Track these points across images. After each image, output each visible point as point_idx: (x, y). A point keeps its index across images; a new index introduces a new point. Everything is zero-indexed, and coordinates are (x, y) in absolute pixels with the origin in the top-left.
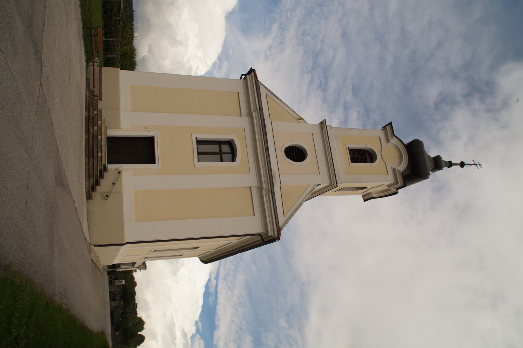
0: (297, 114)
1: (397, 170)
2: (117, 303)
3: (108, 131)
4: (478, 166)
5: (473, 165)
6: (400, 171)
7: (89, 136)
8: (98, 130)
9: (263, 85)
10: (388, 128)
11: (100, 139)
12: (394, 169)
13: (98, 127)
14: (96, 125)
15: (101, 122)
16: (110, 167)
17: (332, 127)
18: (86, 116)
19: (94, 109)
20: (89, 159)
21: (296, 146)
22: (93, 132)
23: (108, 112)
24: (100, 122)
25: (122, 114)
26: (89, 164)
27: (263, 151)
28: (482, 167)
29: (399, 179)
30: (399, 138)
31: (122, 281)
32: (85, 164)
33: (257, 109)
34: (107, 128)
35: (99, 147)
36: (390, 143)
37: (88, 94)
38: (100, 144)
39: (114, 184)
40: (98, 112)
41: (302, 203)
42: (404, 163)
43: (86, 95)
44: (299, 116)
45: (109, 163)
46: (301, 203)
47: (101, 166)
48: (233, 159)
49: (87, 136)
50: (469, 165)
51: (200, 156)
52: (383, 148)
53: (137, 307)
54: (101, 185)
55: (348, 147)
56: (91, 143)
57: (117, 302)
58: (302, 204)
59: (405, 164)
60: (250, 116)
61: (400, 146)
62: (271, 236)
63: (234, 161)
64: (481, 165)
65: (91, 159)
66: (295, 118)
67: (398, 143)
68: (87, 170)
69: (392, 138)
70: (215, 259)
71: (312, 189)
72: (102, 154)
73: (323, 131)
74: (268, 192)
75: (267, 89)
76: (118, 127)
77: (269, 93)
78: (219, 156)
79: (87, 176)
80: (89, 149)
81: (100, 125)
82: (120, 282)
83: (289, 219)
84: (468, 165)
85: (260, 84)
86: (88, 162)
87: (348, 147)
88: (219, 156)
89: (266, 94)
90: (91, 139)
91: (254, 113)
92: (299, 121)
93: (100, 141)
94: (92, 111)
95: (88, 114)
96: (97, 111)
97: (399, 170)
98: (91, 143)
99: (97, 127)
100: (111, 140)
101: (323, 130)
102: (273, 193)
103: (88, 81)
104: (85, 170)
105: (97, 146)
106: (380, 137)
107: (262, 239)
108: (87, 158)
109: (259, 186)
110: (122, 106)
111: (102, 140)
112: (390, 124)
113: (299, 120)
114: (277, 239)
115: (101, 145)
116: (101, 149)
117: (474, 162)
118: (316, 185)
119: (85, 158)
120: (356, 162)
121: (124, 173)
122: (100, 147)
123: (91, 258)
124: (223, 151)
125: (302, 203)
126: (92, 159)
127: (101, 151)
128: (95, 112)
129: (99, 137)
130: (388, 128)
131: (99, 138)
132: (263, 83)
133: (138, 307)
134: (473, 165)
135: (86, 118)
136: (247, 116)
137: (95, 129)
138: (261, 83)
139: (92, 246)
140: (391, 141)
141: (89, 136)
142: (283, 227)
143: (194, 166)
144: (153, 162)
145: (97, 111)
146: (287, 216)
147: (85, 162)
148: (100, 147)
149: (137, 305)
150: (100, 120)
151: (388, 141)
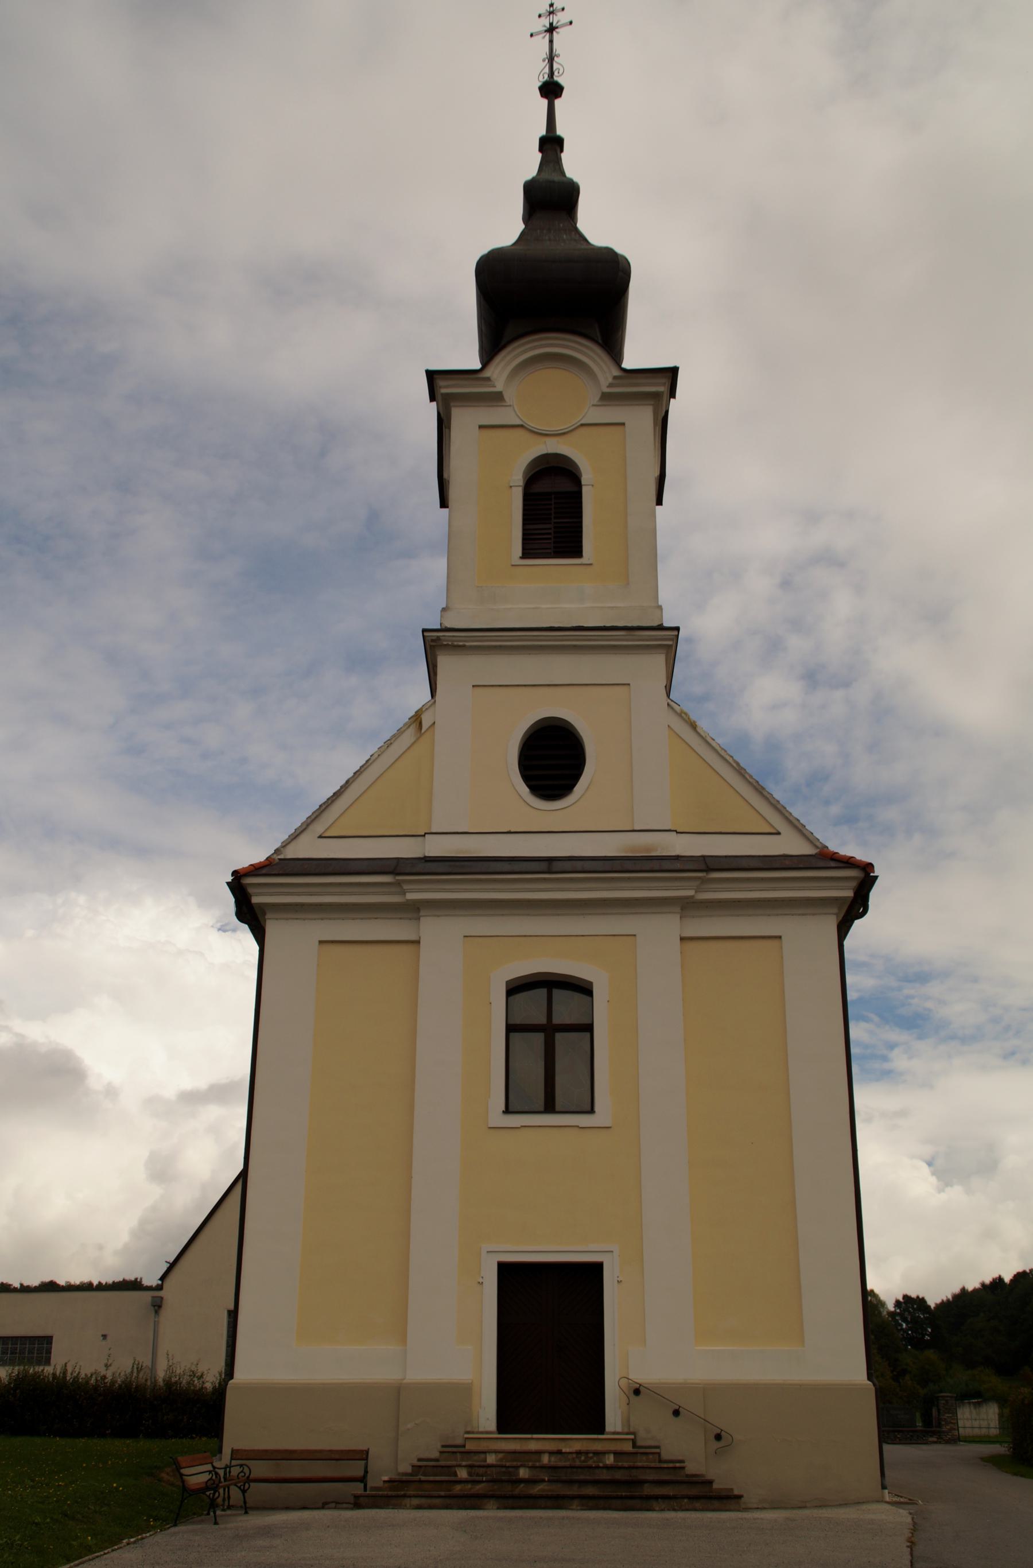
0: (400, 732)
1: (610, 386)
3: (481, 1429)
4: (556, 19)
5: (551, 41)
6: (615, 378)
7: (573, 1497)
8: (530, 1464)
9: (285, 845)
11: (553, 1459)
12: (607, 398)
13: (519, 1464)
14: (511, 1469)
17: (444, 606)
18: (498, 1508)
19: (453, 1478)
20: (656, 1498)
21: (521, 746)
22: (549, 1481)
23: (409, 1426)
24: (488, 1456)
25: (416, 1375)
26: (674, 1498)
27: (558, 880)
28: (560, 7)
29: (644, 385)
32: (674, 1510)
33: (398, 884)
34: (473, 1433)
36: (504, 393)
37: (416, 1501)
38: (570, 1456)
39: (676, 1413)
40: (464, 1463)
41: (735, 765)
42: (584, 354)
43: (419, 1507)
44: (407, 726)
45: (596, 1423)
46: (735, 769)
47: (651, 1456)
48: (585, 989)
49: (576, 1502)
50: (551, 59)
56: (590, 1490)
58: (738, 764)
59: (591, 354)
60: (418, 910)
61: (518, 355)
64: (551, 5)
65: (648, 1490)
66: (413, 740)
67: (508, 358)
68: (698, 1505)
69: (488, 379)
71: (684, 719)
72: (609, 1452)
73: (467, 644)
74: (703, 881)
75: (302, 832)
76: (464, 1391)
77: (319, 828)
78: (559, 1036)
79: (716, 1504)
80: (621, 1497)
81: (501, 1455)
83: (791, 818)
84: (555, 66)
85: (282, 857)
88: (559, 1036)
89: (320, 837)
90: (574, 1490)
91: (410, 896)
92: (425, 726)
93: (559, 1456)
94: (469, 1486)
96: (457, 1469)
97: (610, 380)
98: (590, 1490)
99: (517, 1467)
101: (464, 646)
102: (708, 864)
103: (361, 1499)
104: (695, 1510)
105: (590, 1467)
109: (678, 909)
110: (384, 1373)
111: (559, 1452)
112: (435, 376)
113: (423, 731)
115: (574, 1455)
116: (591, 1455)
117: (538, 33)
118: (668, 704)
119: (653, 1510)
120: (581, 542)
121: (641, 1375)
122: (583, 1458)
124: (543, 1020)
125: (735, 765)
126: (646, 1485)
127: (596, 1453)
128: (463, 1474)
129: (545, 1459)
131: (550, 1461)
132: (278, 845)
134: (551, 41)
135: (506, 1508)
136: (419, 919)
137: (527, 1476)
138: (277, 851)
140: (499, 387)
141: (573, 1497)
142: (818, 844)
144: (597, 1269)
145: (460, 1466)
146: (779, 824)
147: (669, 1510)
148: (583, 1458)
150: (482, 1456)
151: (497, 398)
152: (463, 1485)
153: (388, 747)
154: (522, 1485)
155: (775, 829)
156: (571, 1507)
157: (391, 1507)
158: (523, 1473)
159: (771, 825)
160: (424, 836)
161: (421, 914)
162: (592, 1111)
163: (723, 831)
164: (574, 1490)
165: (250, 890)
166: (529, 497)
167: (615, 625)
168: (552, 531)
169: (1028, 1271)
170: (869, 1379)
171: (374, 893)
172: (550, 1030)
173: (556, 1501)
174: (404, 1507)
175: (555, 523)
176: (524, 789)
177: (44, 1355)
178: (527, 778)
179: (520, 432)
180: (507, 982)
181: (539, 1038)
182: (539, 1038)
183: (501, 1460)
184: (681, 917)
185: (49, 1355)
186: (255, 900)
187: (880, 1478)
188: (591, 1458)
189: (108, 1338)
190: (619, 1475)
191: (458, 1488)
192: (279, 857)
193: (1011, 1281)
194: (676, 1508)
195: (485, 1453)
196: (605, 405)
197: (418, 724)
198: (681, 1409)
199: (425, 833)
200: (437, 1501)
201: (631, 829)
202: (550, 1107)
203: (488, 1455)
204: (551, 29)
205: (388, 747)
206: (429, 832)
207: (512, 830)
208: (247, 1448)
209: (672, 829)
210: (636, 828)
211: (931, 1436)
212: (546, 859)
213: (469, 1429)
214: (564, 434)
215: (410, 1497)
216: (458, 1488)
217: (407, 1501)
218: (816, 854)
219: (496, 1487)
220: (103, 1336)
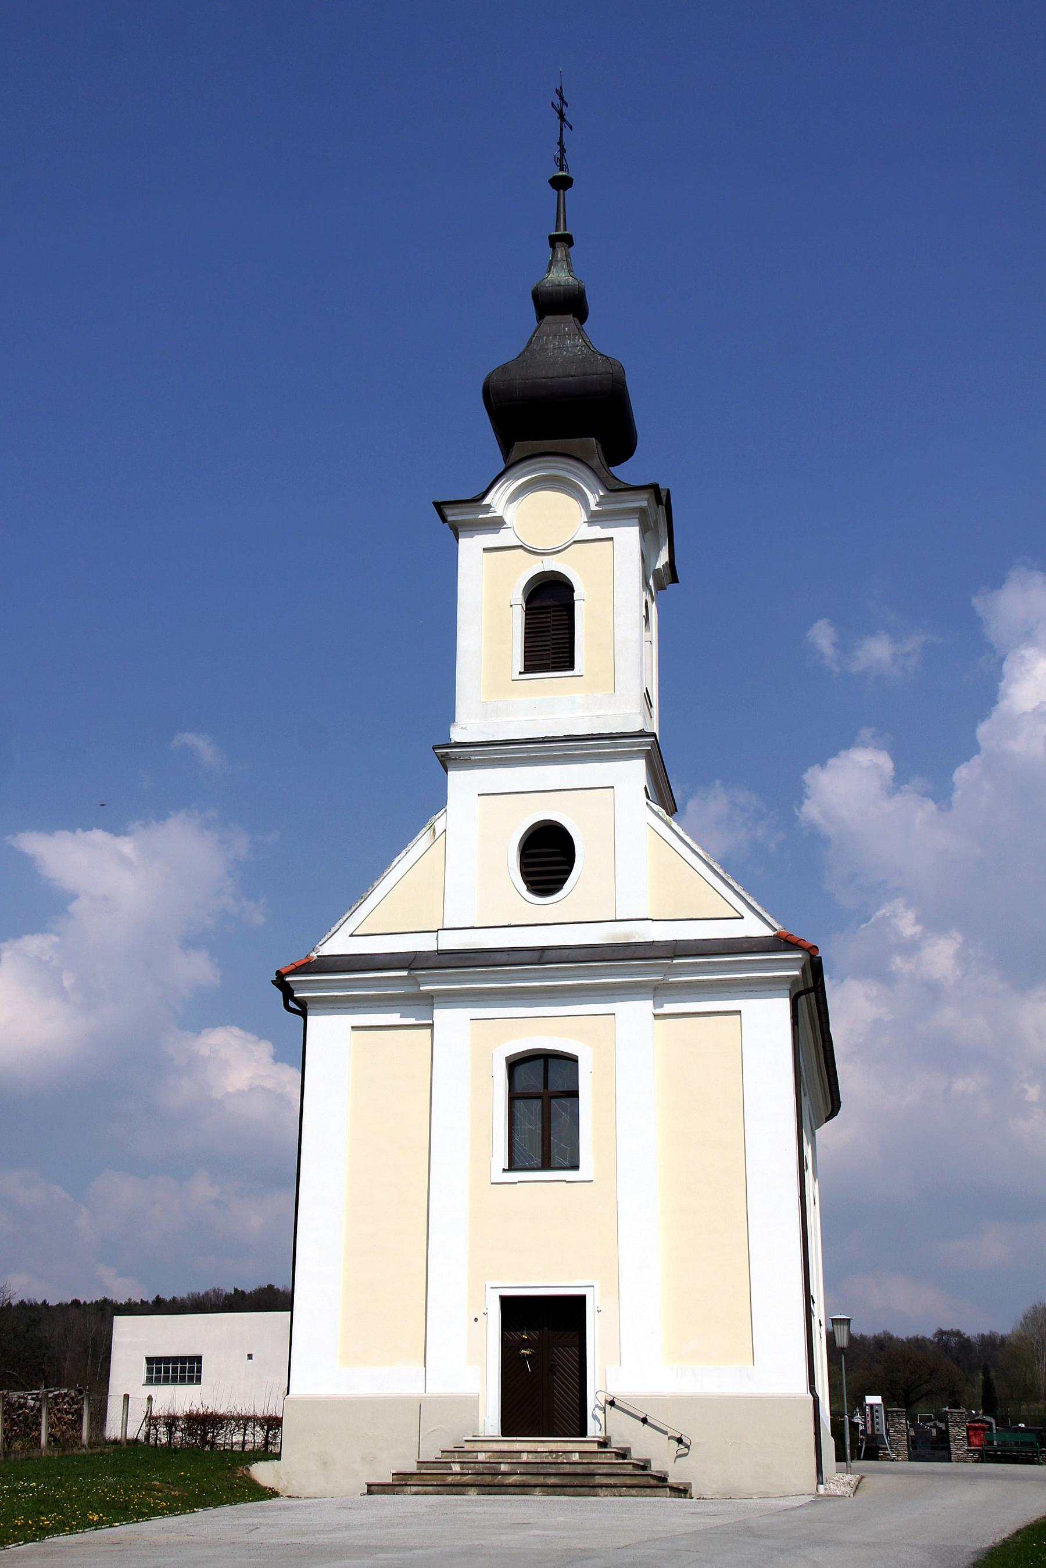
2: (958, 1433)
7: (536, 1486)
10: (453, 515)
15: (523, 1452)
16: (594, 1429)
18: (478, 1494)
19: (449, 1471)
20: (601, 1486)
25: (436, 1389)
30: (491, 481)
31: (871, 1406)
35: (555, 1458)
36: (504, 517)
37: (415, 1489)
49: (538, 1489)
51: (556, 1158)
52: (521, 544)
53: (958, 1334)
54: (648, 1458)
55: (521, 673)
57: (953, 1431)
59: (573, 469)
62: (803, 970)
63: (576, 1059)
65: (598, 1480)
69: (489, 506)
70: (828, 1074)
76: (471, 1403)
82: (872, 1414)
86: (609, 1489)
87: (521, 673)
89: (351, 935)
90: (541, 1480)
94: (459, 1477)
95: (473, 1489)
100: (510, 1426)
106: (485, 550)
107: (806, 991)
108: (599, 1490)
110: (413, 1389)
113: (436, 837)
114: (812, 954)
115: (548, 1454)
118: (647, 804)
121: (618, 1389)
122: (554, 1456)
123: (854, 1495)
124: (539, 1088)
130: (454, 515)
133: (955, 1328)
139: (819, 1490)
141: (536, 1486)
143: (592, 1181)
144: (581, 1300)
147: (611, 1496)
149: (944, 1329)
150: (475, 1454)
151: (497, 524)
152: (454, 1476)
153: (407, 853)
154: (500, 1476)
155: (740, 914)
156: (534, 1493)
158: (504, 1468)
159: (739, 913)
160: (437, 931)
161: (434, 1001)
162: (575, 1167)
163: (694, 917)
164: (541, 1480)
165: (292, 986)
171: (394, 985)
173: (523, 1488)
174: (405, 1493)
176: (522, 887)
177: (170, 1375)
179: (520, 551)
181: (537, 1104)
182: (537, 1104)
183: (490, 1457)
184: (654, 997)
185: (985, 1461)
187: (815, 1475)
188: (561, 1456)
189: (253, 1357)
190: (579, 1469)
191: (450, 1479)
192: (318, 954)
193: (15, 1306)
194: (617, 1494)
195: (477, 1452)
196: (595, 522)
197: (432, 831)
198: (647, 1417)
199: (438, 930)
201: (614, 919)
202: (546, 1165)
205: (407, 853)
206: (441, 928)
207: (512, 924)
208: (107, 1414)
209: (649, 918)
210: (618, 918)
212: (540, 948)
213: (475, 1434)
214: (559, 551)
215: (410, 1485)
216: (450, 1479)
218: (774, 935)
219: (479, 1478)
220: (248, 1355)
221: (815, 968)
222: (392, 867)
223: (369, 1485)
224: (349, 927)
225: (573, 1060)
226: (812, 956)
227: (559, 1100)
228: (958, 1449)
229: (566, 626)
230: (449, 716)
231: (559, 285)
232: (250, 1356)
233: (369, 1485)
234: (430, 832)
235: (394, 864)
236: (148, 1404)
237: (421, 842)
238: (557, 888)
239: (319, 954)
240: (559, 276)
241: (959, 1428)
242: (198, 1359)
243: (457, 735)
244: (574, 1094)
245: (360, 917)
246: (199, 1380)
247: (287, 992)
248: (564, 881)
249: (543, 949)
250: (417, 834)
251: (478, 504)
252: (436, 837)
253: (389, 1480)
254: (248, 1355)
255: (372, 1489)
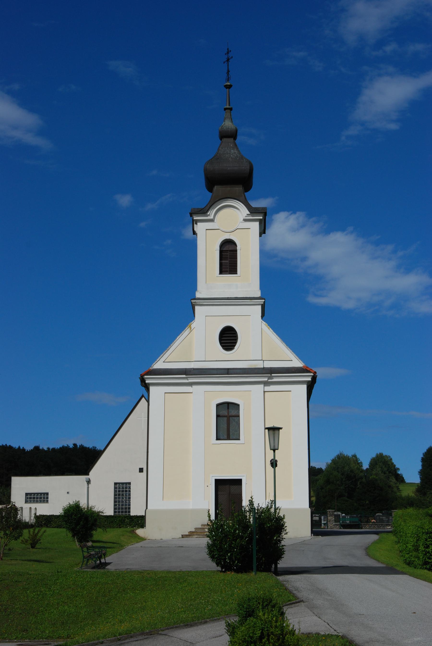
6: (247, 214)
19: (205, 531)
37: (196, 536)
113: (192, 330)
157: (313, 499)
166: (221, 252)
167: (246, 297)
168: (228, 263)
169: (394, 464)
170: (310, 507)
172: (229, 417)
175: (229, 269)
176: (221, 348)
178: (221, 343)
180: (216, 404)
186: (147, 382)
189: (69, 493)
200: (201, 536)
202: (229, 438)
203: (107, 550)
204: (228, 60)
211: (389, 526)
217: (194, 536)
220: (69, 494)
221: (314, 378)
222: (177, 339)
223: (182, 535)
224: (163, 359)
225: (238, 405)
226: (314, 375)
227: (233, 418)
228: (331, 524)
229: (224, 252)
230: (195, 288)
231: (229, 128)
232: (68, 493)
233: (182, 535)
234: (189, 329)
235: (177, 338)
236: (35, 511)
237: (186, 332)
238: (232, 348)
239: (153, 368)
240: (228, 124)
241: (332, 517)
242: (47, 494)
243: (198, 295)
244: (239, 416)
245: (166, 356)
246: (47, 502)
247: (143, 381)
248: (234, 346)
249: (228, 369)
250: (185, 329)
251: (206, 214)
252: (192, 330)
253: (187, 534)
254: (69, 494)
255: (183, 536)
